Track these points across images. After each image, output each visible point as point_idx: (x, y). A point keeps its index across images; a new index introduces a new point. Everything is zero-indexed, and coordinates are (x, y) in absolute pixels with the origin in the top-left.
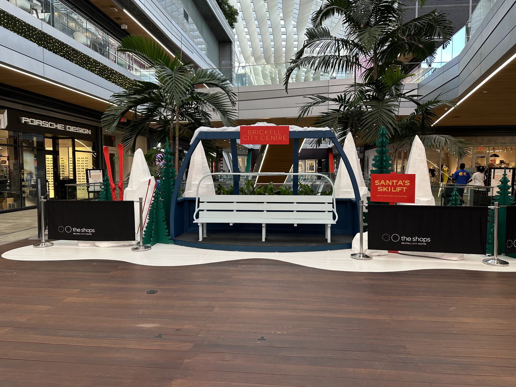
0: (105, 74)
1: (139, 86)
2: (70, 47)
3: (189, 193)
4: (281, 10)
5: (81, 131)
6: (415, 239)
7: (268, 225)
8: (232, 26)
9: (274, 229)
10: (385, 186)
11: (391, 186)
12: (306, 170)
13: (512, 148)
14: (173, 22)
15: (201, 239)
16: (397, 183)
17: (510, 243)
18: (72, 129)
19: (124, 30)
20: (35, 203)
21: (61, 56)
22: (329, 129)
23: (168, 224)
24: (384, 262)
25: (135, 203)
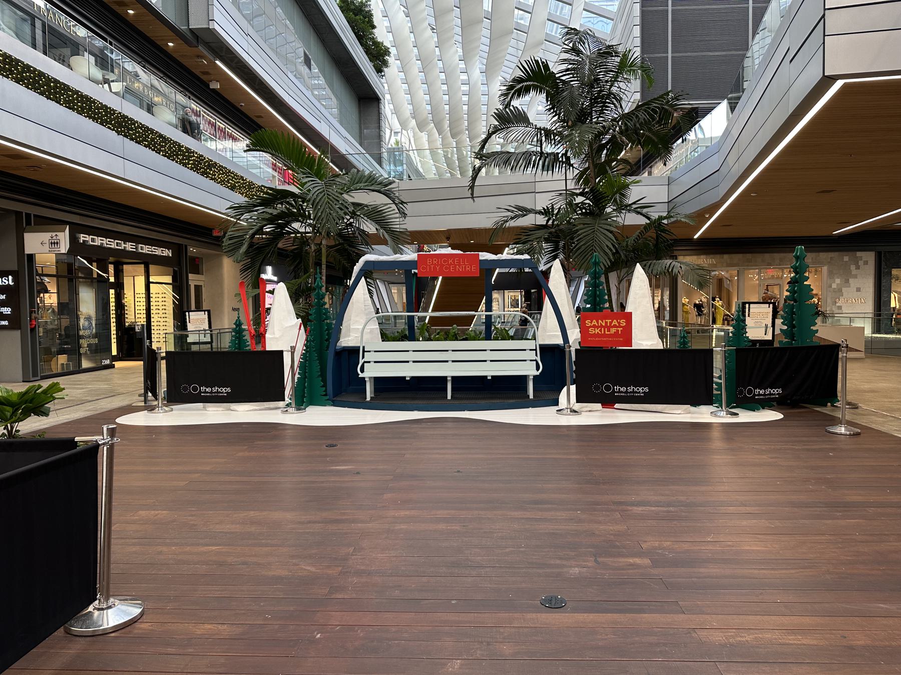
0: (201, 168)
1: (267, 193)
2: (157, 132)
3: (347, 340)
4: (460, 45)
5: (159, 251)
6: (630, 389)
7: (453, 378)
8: (379, 70)
9: (461, 383)
10: (598, 327)
11: (604, 327)
12: (505, 305)
13: (816, 271)
14: (290, 75)
15: (368, 399)
16: (611, 323)
17: (741, 392)
18: (146, 249)
19: (214, 90)
20: (96, 362)
21: (146, 146)
22: (529, 257)
23: (324, 380)
24: (594, 415)
25: (285, 353)
